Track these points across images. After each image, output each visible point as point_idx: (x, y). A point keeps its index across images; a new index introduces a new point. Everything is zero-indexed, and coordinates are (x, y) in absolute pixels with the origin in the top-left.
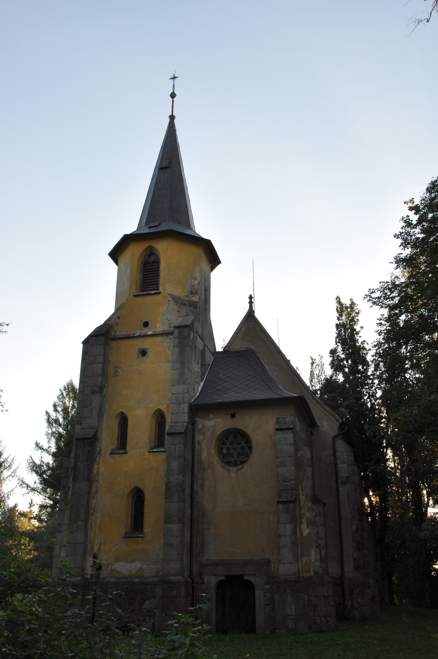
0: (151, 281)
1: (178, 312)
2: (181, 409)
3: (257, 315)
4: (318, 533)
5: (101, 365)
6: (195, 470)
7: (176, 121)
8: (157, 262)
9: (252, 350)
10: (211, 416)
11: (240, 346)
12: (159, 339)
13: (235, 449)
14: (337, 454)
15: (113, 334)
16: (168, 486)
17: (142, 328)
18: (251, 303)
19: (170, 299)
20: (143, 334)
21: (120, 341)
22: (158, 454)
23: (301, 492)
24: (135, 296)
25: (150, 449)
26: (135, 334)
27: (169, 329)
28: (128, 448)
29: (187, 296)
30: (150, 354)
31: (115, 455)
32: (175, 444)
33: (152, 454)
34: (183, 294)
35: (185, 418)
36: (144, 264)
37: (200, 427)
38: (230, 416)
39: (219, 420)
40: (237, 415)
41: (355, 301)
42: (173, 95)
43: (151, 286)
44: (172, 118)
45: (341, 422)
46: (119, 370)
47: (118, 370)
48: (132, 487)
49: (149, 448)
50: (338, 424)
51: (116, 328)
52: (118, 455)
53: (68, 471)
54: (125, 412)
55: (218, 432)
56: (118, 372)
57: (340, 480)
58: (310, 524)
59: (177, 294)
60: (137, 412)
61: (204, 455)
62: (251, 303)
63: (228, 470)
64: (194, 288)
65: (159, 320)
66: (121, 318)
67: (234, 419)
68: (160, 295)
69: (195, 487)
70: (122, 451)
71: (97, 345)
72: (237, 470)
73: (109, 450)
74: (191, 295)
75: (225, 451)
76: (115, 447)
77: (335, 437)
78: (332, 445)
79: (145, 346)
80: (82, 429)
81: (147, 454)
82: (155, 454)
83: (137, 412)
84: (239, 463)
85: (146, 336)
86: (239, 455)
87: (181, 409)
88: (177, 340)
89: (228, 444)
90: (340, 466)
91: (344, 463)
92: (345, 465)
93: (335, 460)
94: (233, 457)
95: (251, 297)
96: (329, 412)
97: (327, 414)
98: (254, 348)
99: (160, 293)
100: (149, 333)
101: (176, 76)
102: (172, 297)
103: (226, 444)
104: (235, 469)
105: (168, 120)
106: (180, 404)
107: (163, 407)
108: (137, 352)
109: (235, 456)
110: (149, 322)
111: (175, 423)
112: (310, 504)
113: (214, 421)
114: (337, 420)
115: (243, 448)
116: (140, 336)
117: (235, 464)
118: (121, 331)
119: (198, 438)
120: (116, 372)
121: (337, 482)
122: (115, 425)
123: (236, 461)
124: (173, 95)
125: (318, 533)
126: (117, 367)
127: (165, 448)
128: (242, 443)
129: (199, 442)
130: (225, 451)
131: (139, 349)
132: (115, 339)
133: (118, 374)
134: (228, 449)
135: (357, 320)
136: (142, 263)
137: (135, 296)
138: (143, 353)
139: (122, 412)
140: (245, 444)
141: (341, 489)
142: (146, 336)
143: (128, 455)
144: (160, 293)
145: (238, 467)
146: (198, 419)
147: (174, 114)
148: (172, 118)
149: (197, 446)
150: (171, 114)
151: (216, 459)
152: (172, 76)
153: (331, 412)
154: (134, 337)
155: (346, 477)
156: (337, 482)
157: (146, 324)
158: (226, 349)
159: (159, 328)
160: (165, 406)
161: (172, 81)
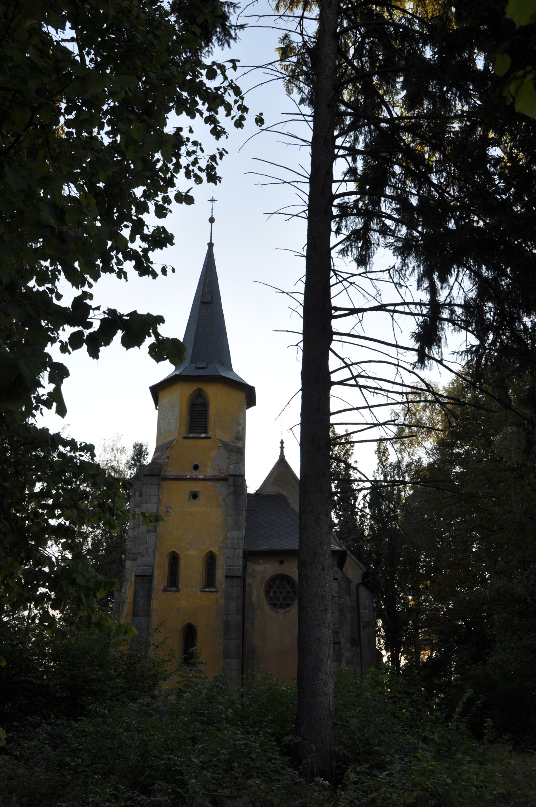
0: (199, 423)
1: (228, 458)
2: (236, 553)
3: (287, 458)
4: (355, 671)
5: (156, 505)
6: (246, 611)
7: (215, 249)
8: (205, 405)
9: (283, 495)
10: (261, 561)
11: (272, 490)
12: (210, 483)
13: (281, 593)
14: (360, 600)
15: (162, 473)
16: (227, 625)
17: (193, 471)
18: (282, 448)
19: (220, 445)
20: (194, 477)
21: (170, 482)
22: (210, 594)
23: (341, 634)
24: (184, 438)
25: (202, 588)
26: (186, 476)
27: (220, 474)
28: (180, 587)
29: (233, 442)
30: (201, 497)
31: (167, 593)
32: (233, 587)
33: (204, 593)
34: (230, 440)
35: (240, 562)
36: (192, 406)
37: (250, 570)
38: (278, 563)
39: (268, 566)
40: (285, 562)
41: (147, 278)
42: (212, 220)
43: (198, 428)
44: (211, 245)
45: (365, 571)
46: (171, 511)
47: (169, 510)
48: (185, 623)
49: (201, 587)
50: (362, 573)
51: (165, 468)
52: (170, 593)
53: (119, 606)
54: (177, 552)
55: (267, 577)
56: (169, 512)
57: (361, 624)
58: (349, 662)
59: (224, 440)
60: (189, 552)
61: (254, 598)
62: (282, 448)
63: (277, 612)
64: (239, 433)
65: (210, 464)
66: (170, 458)
67: (282, 566)
68: (210, 440)
69: (246, 626)
70: (174, 589)
71: (151, 485)
72: (285, 613)
73: (162, 588)
74: (236, 441)
75: (271, 594)
76: (165, 584)
77: (359, 584)
78: (355, 592)
79: (196, 490)
80: (138, 566)
81: (199, 593)
82: (207, 594)
83: (189, 552)
84: (285, 606)
85: (197, 479)
86: (284, 598)
87: (236, 553)
88: (232, 488)
89: (275, 588)
90: (362, 611)
91: (366, 609)
92: (367, 611)
93: (358, 606)
94: (279, 600)
95: (282, 442)
96: (354, 561)
97: (352, 562)
98: (284, 493)
99: (210, 438)
100: (201, 477)
101: (215, 198)
102: (222, 444)
103: (272, 588)
104: (283, 611)
105: (207, 248)
106: (235, 549)
107: (215, 550)
108: (189, 494)
109: (281, 600)
110: (200, 465)
111: (230, 566)
112: (349, 646)
113: (263, 566)
114: (361, 569)
115: (288, 592)
116: (191, 479)
117: (281, 607)
118: (170, 471)
119: (249, 581)
120: (167, 511)
121: (359, 626)
122: (166, 563)
123: (281, 604)
124: (212, 220)
125: (355, 671)
126: (168, 507)
127: (216, 588)
128: (288, 588)
129: (250, 585)
130: (271, 594)
131: (191, 492)
132: (166, 479)
133: (169, 514)
134: (275, 592)
135: (352, 453)
136: (189, 404)
137: (184, 438)
138: (195, 496)
139: (174, 551)
140: (290, 588)
141: (362, 632)
142: (197, 479)
143: (181, 593)
144: (210, 438)
145: (286, 610)
146: (248, 563)
147: (213, 242)
148: (211, 245)
149: (247, 588)
150: (209, 242)
151: (264, 601)
152: (211, 198)
153: (356, 561)
154: (185, 479)
155: (368, 622)
156: (359, 626)
157: (196, 467)
158: (258, 493)
159: (210, 472)
160: (217, 549)
161: (211, 203)
